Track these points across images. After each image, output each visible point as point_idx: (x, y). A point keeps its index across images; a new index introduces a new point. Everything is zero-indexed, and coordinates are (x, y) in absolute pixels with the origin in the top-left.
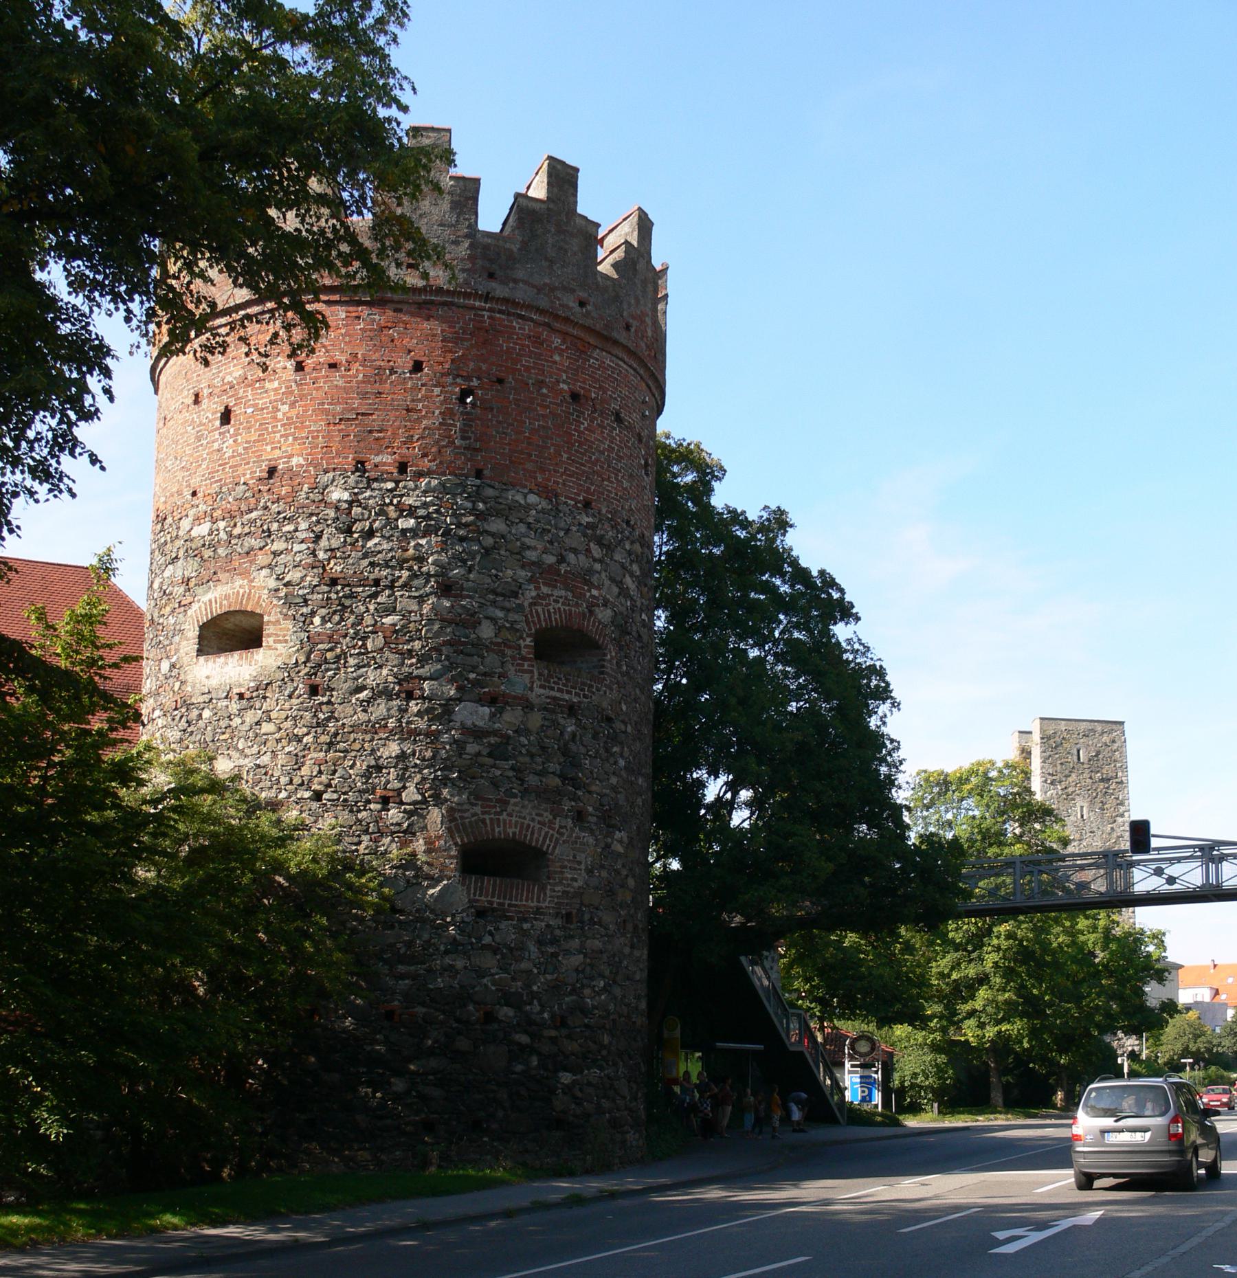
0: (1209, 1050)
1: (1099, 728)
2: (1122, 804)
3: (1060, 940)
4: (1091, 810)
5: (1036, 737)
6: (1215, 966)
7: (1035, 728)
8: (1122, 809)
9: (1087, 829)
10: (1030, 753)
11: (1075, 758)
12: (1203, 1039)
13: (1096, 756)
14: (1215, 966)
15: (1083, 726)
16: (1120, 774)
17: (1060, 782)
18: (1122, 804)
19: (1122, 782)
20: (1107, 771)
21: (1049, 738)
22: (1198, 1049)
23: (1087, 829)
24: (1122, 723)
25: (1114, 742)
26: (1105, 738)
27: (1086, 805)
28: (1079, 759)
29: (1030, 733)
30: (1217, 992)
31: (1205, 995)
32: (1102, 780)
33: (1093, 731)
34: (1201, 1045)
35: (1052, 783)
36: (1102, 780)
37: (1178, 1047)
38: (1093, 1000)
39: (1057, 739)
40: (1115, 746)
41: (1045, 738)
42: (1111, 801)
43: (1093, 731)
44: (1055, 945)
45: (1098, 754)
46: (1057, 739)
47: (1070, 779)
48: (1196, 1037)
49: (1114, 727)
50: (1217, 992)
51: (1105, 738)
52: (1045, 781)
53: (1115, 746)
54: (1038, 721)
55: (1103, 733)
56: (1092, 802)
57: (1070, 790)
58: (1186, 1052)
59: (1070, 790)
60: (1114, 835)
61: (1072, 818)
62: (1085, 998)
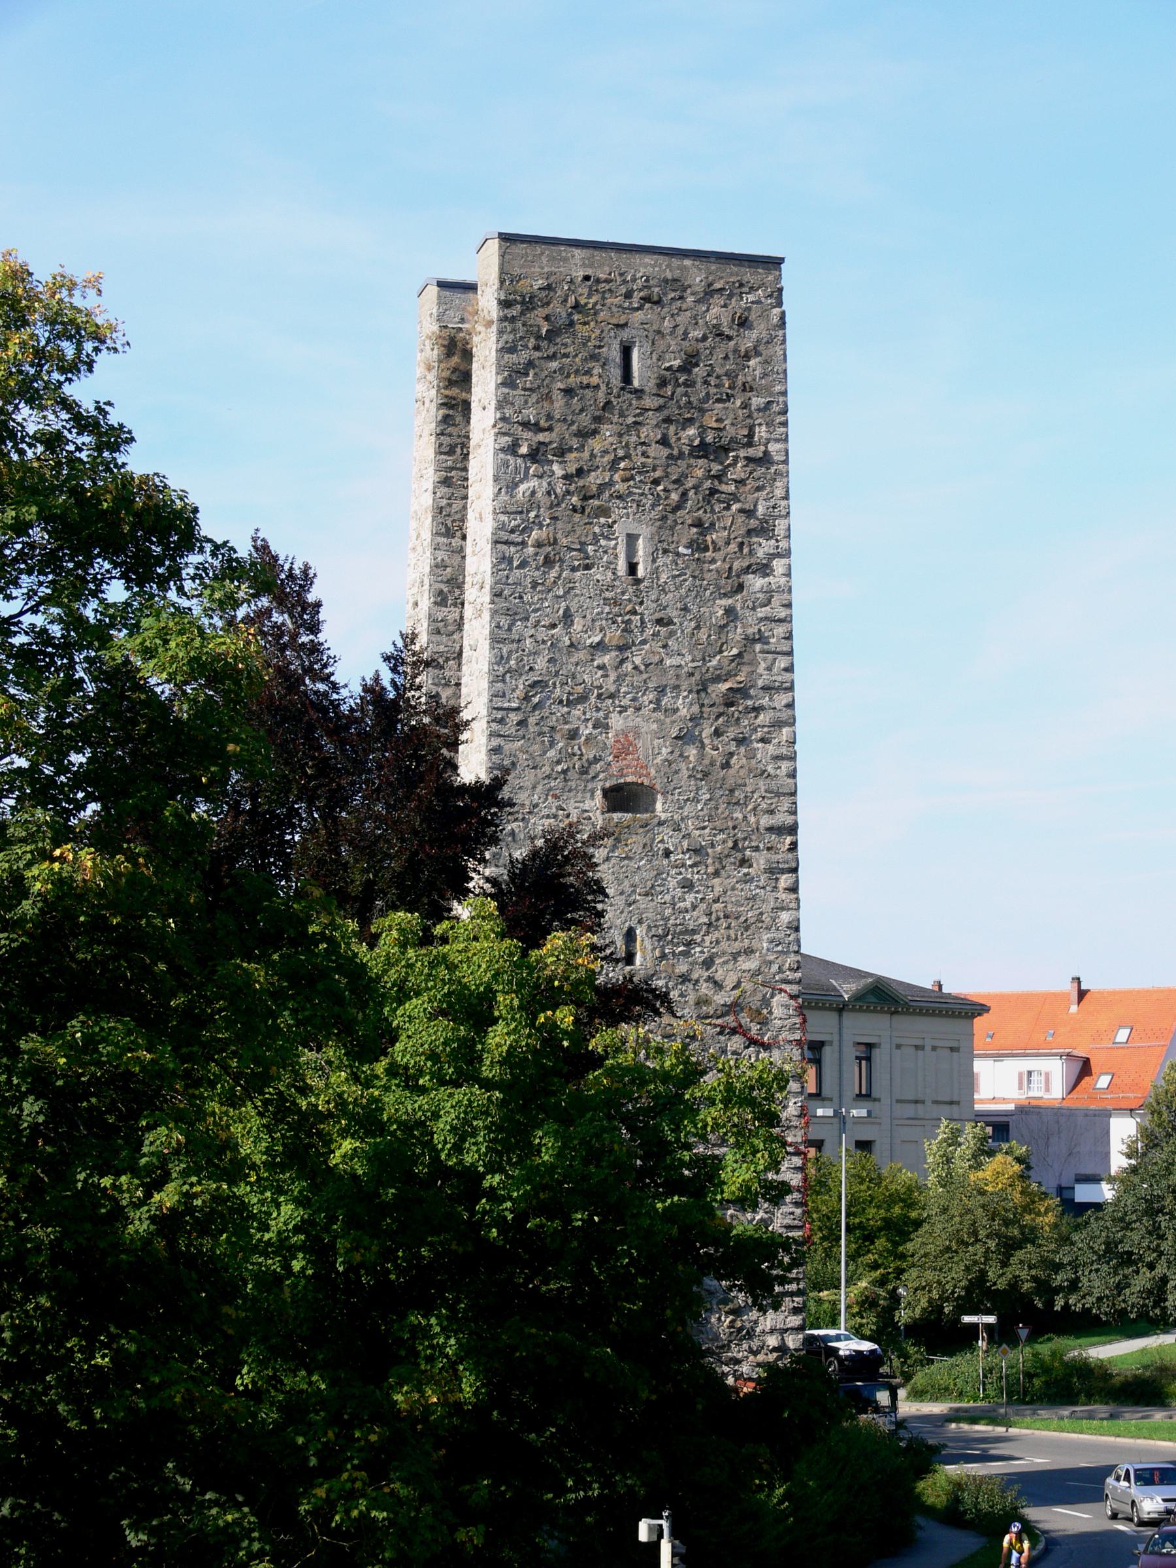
0: (1045, 1289)
1: (697, 278)
2: (765, 530)
3: (167, 1197)
4: (661, 548)
5: (488, 301)
6: (1082, 994)
7: (484, 268)
8: (764, 547)
9: (648, 610)
10: (468, 355)
11: (615, 374)
12: (1027, 1253)
13: (686, 368)
14: (1082, 994)
15: (645, 267)
16: (761, 432)
17: (561, 453)
18: (765, 530)
19: (765, 460)
20: (722, 418)
21: (529, 303)
22: (1015, 1284)
23: (648, 610)
24: (774, 263)
25: (744, 323)
26: (716, 313)
27: (644, 532)
28: (627, 376)
29: (471, 288)
30: (1085, 1069)
31: (1049, 1081)
32: (702, 450)
33: (677, 285)
34: (1021, 1269)
35: (534, 455)
36: (702, 450)
37: (956, 1277)
38: (351, 1496)
39: (556, 308)
40: (748, 340)
41: (517, 304)
42: (728, 524)
43: (677, 285)
44: (139, 1224)
45: (691, 361)
46: (556, 308)
47: (595, 444)
48: (1009, 1247)
49: (748, 275)
50: (1085, 1069)
51: (716, 313)
52: (512, 449)
53: (748, 340)
54: (494, 246)
55: (710, 292)
56: (666, 521)
57: (594, 479)
58: (978, 1294)
59: (594, 479)
60: (737, 634)
61: (597, 574)
62: (310, 1478)
